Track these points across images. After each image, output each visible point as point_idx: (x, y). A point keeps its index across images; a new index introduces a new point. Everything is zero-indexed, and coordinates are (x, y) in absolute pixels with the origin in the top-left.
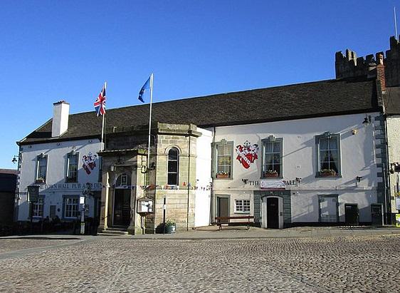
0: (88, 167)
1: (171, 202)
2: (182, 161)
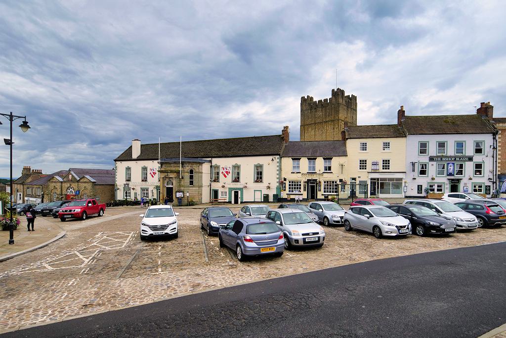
0: (153, 174)
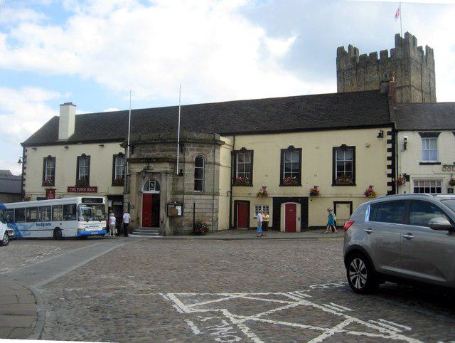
1: (199, 206)
2: (207, 169)
